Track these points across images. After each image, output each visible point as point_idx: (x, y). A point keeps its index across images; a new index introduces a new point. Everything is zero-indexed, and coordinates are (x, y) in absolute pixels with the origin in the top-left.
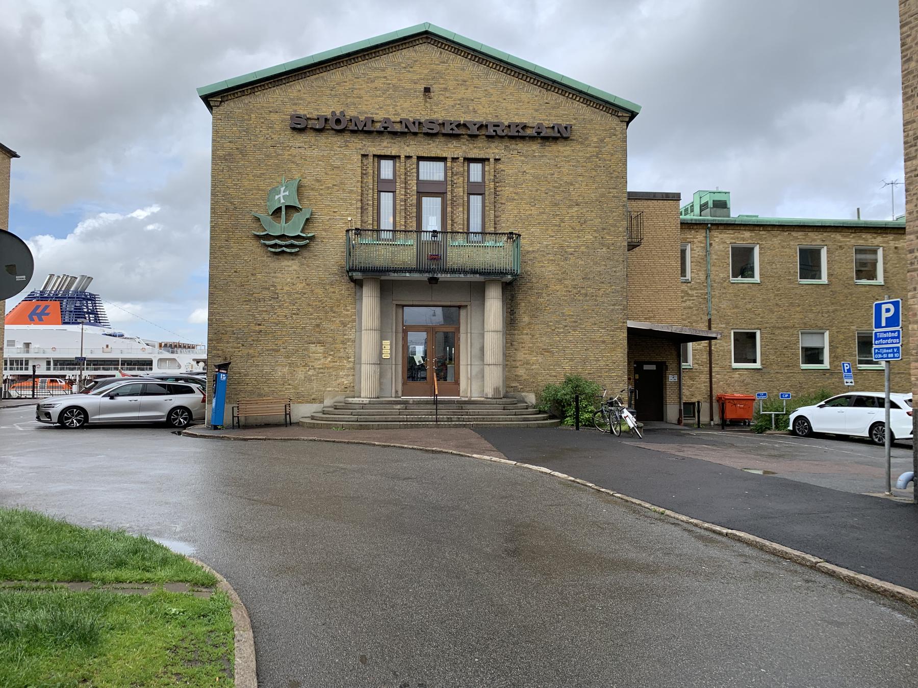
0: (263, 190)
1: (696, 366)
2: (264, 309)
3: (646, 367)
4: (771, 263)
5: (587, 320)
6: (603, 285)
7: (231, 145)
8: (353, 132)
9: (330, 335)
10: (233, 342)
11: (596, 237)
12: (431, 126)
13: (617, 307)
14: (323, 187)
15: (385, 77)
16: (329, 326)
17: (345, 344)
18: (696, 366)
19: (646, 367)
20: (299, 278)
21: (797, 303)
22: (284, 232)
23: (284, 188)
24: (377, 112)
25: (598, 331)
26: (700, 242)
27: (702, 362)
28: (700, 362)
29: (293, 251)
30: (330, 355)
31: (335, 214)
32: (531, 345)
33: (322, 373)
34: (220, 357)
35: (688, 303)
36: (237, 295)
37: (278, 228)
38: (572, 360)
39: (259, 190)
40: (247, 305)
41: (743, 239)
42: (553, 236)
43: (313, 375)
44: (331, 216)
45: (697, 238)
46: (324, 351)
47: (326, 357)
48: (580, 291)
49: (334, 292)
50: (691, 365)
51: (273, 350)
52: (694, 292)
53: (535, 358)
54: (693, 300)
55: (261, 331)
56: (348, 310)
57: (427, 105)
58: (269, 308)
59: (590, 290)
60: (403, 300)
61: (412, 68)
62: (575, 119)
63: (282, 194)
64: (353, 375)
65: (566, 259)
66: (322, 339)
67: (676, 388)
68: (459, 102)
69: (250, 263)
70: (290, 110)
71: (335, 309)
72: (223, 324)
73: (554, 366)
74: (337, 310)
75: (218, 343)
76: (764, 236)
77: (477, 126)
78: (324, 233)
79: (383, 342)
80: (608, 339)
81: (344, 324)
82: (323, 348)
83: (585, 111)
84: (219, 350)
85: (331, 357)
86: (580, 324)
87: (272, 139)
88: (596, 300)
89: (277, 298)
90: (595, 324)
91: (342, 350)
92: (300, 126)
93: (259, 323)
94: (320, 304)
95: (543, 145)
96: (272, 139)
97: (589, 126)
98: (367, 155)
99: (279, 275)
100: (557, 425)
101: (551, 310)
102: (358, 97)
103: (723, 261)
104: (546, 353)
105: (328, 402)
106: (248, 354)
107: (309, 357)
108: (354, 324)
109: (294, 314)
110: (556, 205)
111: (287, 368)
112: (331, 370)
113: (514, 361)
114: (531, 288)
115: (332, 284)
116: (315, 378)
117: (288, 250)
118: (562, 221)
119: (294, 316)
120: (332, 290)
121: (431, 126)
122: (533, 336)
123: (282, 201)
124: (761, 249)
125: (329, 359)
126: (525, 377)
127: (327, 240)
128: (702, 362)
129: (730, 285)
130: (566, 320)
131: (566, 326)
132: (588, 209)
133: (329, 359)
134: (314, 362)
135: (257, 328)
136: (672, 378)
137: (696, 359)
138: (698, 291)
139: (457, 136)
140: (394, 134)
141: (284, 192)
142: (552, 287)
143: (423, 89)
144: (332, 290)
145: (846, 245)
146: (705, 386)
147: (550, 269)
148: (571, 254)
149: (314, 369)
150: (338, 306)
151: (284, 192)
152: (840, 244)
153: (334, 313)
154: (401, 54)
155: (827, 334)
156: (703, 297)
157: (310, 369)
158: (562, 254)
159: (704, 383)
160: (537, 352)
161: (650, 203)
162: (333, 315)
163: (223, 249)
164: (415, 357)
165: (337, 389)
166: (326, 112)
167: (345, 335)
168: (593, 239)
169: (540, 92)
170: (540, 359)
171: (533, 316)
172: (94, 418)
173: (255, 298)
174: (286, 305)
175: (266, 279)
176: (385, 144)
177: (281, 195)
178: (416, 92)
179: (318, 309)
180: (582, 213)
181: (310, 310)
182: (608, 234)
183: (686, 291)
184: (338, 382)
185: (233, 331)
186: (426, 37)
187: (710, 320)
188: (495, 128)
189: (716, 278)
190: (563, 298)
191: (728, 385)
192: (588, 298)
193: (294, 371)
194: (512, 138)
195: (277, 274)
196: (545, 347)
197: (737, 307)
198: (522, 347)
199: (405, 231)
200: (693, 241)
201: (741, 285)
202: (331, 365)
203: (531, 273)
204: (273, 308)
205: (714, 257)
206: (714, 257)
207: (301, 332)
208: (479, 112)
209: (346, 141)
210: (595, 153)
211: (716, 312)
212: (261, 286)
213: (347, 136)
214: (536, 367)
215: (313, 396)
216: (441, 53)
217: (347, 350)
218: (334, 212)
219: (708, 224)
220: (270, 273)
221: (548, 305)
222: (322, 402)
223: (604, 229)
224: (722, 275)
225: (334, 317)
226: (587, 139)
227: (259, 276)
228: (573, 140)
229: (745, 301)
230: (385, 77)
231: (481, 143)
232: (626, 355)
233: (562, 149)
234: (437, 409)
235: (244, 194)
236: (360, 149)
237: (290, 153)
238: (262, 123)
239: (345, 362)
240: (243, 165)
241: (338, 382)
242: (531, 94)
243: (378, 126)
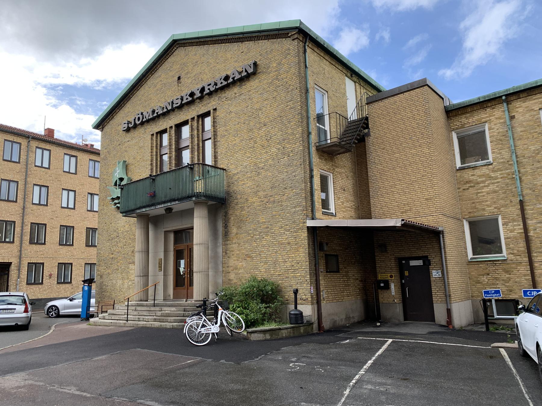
1: (512, 257)
3: (413, 263)
5: (275, 225)
6: (286, 190)
11: (279, 149)
13: (297, 209)
15: (161, 81)
18: (512, 257)
19: (413, 263)
26: (499, 118)
27: (518, 251)
28: (515, 251)
32: (238, 252)
35: (491, 187)
38: (266, 263)
42: (249, 157)
45: (494, 115)
50: (506, 256)
52: (498, 174)
53: (241, 264)
54: (498, 182)
57: (179, 88)
59: (277, 197)
67: (440, 284)
80: (291, 240)
83: (265, 45)
86: (271, 229)
88: (281, 206)
90: (282, 227)
95: (241, 86)
103: (532, 131)
104: (248, 259)
110: (251, 130)
114: (237, 204)
118: (255, 143)
126: (235, 281)
128: (518, 251)
136: (435, 274)
137: (510, 248)
138: (503, 172)
142: (251, 200)
146: (526, 280)
148: (262, 169)
154: (168, 62)
156: (509, 177)
158: (255, 170)
159: (525, 275)
160: (242, 258)
161: (396, 98)
164: (180, 268)
170: (244, 264)
171: (239, 227)
172: (62, 312)
180: (268, 131)
182: (288, 143)
183: (488, 174)
187: (521, 203)
192: (275, 205)
200: (490, 120)
206: (519, 129)
209: (146, 129)
211: (530, 192)
214: (242, 271)
219: (501, 97)
223: (284, 140)
224: (533, 148)
228: (260, 73)
232: (307, 254)
233: (253, 84)
234: (128, 310)
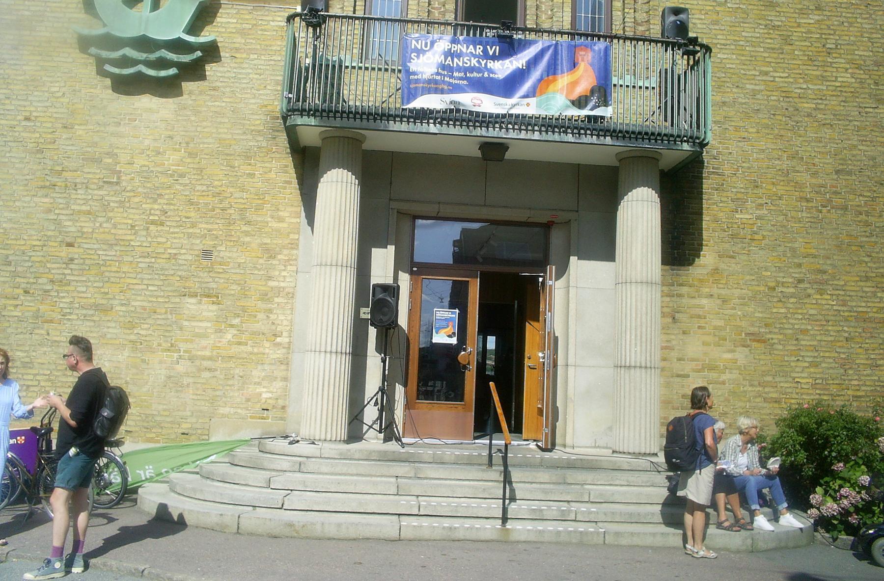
2: (84, 208)
5: (848, 269)
9: (235, 277)
16: (235, 255)
17: (270, 301)
20: (171, 137)
25: (874, 294)
29: (163, 73)
30: (232, 326)
33: (210, 370)
36: (26, 172)
40: (46, 196)
43: (187, 374)
46: (218, 317)
47: (221, 331)
48: (830, 201)
49: (251, 175)
55: (72, 260)
56: (281, 220)
64: (285, 379)
66: (213, 285)
69: (65, 100)
71: (250, 215)
73: (774, 376)
74: (255, 218)
78: (239, 40)
79: (454, 341)
81: (270, 253)
82: (215, 307)
85: (233, 331)
86: (834, 278)
89: (117, 183)
90: (867, 278)
93: (69, 240)
94: (216, 199)
100: (827, 545)
101: (766, 241)
104: (755, 344)
106: (37, 315)
107: (181, 329)
108: (295, 252)
109: (153, 223)
111: (126, 353)
112: (231, 364)
113: (679, 359)
115: (247, 156)
116: (191, 380)
119: (152, 227)
120: (248, 170)
122: (724, 301)
125: (229, 336)
127: (244, 56)
130: (800, 265)
131: (800, 281)
132: (841, 19)
133: (229, 336)
134: (192, 341)
135: (64, 252)
144: (248, 170)
147: (762, 145)
149: (192, 359)
150: (259, 208)
153: (249, 223)
162: (244, 228)
167: (270, 278)
168: (856, 85)
174: (137, 200)
175: (96, 139)
179: (211, 214)
181: (192, 214)
185: (7, 256)
190: (794, 214)
193: (143, 361)
195: (121, 129)
198: (699, 327)
199: (428, 23)
202: (235, 349)
203: (719, 153)
204: (106, 207)
207: (167, 266)
214: (734, 376)
215: (185, 427)
217: (272, 317)
221: (760, 228)
225: (247, 233)
227: (80, 131)
239: (267, 344)
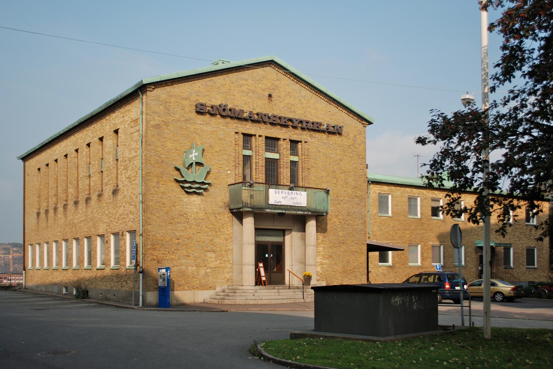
0: (179, 150)
4: (396, 205)
7: (160, 119)
8: (232, 118)
10: (163, 250)
11: (353, 192)
12: (274, 119)
14: (214, 151)
15: (247, 85)
21: (407, 229)
22: (195, 179)
23: (195, 150)
24: (243, 106)
30: (219, 259)
31: (221, 169)
34: (155, 260)
37: (190, 176)
39: (177, 150)
40: (171, 226)
41: (384, 191)
44: (219, 170)
49: (220, 219)
51: (187, 256)
55: (179, 243)
56: (228, 231)
58: (183, 229)
60: (258, 225)
61: (262, 81)
62: (343, 122)
63: (194, 154)
65: (339, 204)
66: (214, 249)
68: (287, 106)
70: (194, 98)
72: (156, 239)
75: (153, 251)
76: (393, 190)
77: (298, 122)
81: (226, 240)
84: (154, 255)
87: (184, 117)
91: (225, 256)
92: (201, 110)
94: (213, 226)
96: (184, 117)
97: (349, 128)
98: (238, 133)
99: (189, 207)
102: (233, 96)
105: (218, 289)
107: (207, 260)
109: (198, 232)
117: (198, 191)
119: (198, 233)
121: (274, 119)
123: (194, 159)
124: (392, 197)
129: (378, 217)
135: (177, 241)
139: (286, 126)
140: (254, 121)
141: (195, 153)
143: (268, 95)
145: (428, 197)
148: (342, 201)
151: (195, 153)
152: (425, 196)
153: (221, 232)
155: (419, 246)
157: (208, 268)
163: (156, 188)
165: (223, 281)
166: (217, 103)
167: (227, 246)
169: (326, 104)
173: (175, 221)
176: (247, 127)
177: (193, 155)
178: (264, 96)
182: (358, 190)
184: (224, 276)
186: (271, 63)
188: (307, 124)
189: (372, 213)
191: (377, 275)
194: (314, 130)
196: (330, 255)
197: (381, 230)
201: (383, 217)
205: (371, 201)
208: (296, 112)
210: (352, 144)
212: (179, 214)
213: (228, 120)
215: (210, 286)
216: (277, 74)
217: (228, 256)
218: (220, 167)
220: (184, 205)
222: (215, 289)
225: (221, 235)
226: (348, 135)
229: (385, 227)
230: (247, 85)
231: (299, 131)
235: (168, 152)
236: (234, 128)
237: (194, 127)
238: (178, 106)
239: (227, 263)
240: (167, 132)
241: (224, 276)
242: (322, 103)
243: (246, 115)
